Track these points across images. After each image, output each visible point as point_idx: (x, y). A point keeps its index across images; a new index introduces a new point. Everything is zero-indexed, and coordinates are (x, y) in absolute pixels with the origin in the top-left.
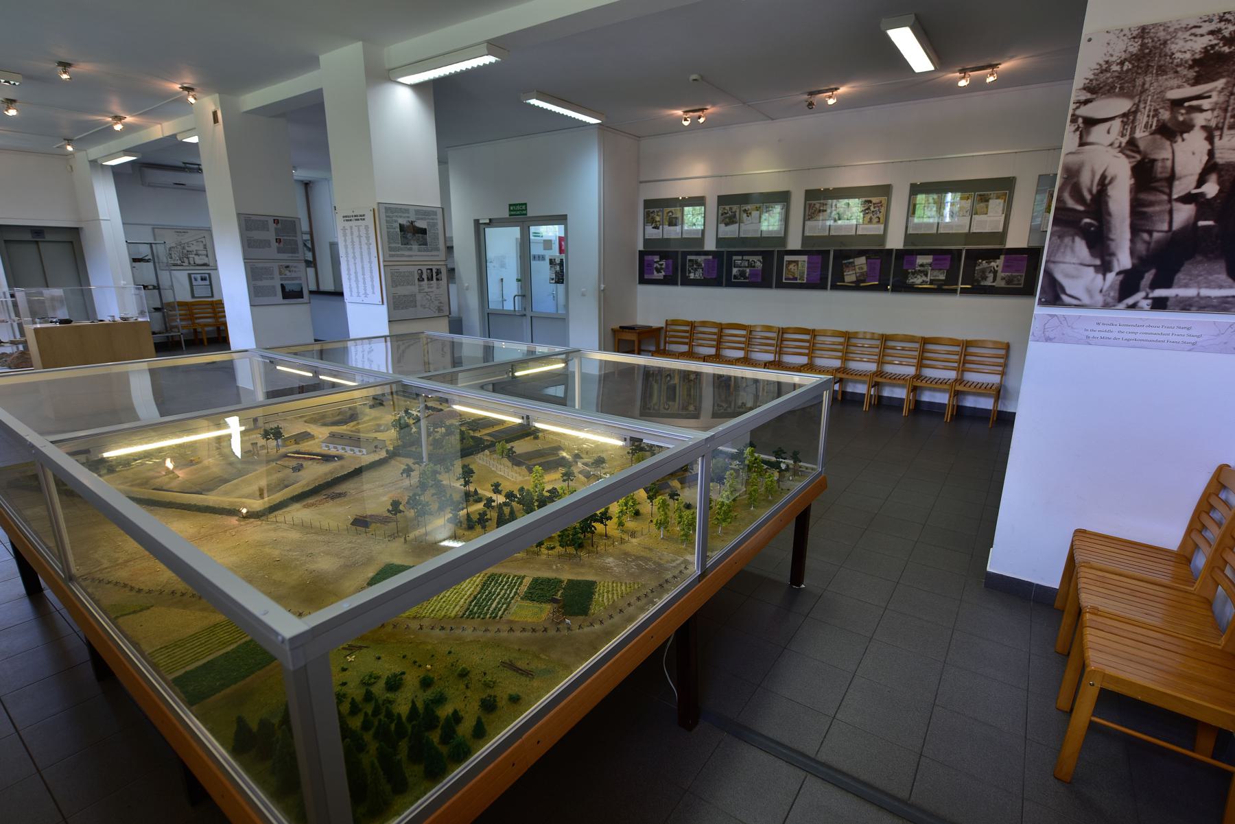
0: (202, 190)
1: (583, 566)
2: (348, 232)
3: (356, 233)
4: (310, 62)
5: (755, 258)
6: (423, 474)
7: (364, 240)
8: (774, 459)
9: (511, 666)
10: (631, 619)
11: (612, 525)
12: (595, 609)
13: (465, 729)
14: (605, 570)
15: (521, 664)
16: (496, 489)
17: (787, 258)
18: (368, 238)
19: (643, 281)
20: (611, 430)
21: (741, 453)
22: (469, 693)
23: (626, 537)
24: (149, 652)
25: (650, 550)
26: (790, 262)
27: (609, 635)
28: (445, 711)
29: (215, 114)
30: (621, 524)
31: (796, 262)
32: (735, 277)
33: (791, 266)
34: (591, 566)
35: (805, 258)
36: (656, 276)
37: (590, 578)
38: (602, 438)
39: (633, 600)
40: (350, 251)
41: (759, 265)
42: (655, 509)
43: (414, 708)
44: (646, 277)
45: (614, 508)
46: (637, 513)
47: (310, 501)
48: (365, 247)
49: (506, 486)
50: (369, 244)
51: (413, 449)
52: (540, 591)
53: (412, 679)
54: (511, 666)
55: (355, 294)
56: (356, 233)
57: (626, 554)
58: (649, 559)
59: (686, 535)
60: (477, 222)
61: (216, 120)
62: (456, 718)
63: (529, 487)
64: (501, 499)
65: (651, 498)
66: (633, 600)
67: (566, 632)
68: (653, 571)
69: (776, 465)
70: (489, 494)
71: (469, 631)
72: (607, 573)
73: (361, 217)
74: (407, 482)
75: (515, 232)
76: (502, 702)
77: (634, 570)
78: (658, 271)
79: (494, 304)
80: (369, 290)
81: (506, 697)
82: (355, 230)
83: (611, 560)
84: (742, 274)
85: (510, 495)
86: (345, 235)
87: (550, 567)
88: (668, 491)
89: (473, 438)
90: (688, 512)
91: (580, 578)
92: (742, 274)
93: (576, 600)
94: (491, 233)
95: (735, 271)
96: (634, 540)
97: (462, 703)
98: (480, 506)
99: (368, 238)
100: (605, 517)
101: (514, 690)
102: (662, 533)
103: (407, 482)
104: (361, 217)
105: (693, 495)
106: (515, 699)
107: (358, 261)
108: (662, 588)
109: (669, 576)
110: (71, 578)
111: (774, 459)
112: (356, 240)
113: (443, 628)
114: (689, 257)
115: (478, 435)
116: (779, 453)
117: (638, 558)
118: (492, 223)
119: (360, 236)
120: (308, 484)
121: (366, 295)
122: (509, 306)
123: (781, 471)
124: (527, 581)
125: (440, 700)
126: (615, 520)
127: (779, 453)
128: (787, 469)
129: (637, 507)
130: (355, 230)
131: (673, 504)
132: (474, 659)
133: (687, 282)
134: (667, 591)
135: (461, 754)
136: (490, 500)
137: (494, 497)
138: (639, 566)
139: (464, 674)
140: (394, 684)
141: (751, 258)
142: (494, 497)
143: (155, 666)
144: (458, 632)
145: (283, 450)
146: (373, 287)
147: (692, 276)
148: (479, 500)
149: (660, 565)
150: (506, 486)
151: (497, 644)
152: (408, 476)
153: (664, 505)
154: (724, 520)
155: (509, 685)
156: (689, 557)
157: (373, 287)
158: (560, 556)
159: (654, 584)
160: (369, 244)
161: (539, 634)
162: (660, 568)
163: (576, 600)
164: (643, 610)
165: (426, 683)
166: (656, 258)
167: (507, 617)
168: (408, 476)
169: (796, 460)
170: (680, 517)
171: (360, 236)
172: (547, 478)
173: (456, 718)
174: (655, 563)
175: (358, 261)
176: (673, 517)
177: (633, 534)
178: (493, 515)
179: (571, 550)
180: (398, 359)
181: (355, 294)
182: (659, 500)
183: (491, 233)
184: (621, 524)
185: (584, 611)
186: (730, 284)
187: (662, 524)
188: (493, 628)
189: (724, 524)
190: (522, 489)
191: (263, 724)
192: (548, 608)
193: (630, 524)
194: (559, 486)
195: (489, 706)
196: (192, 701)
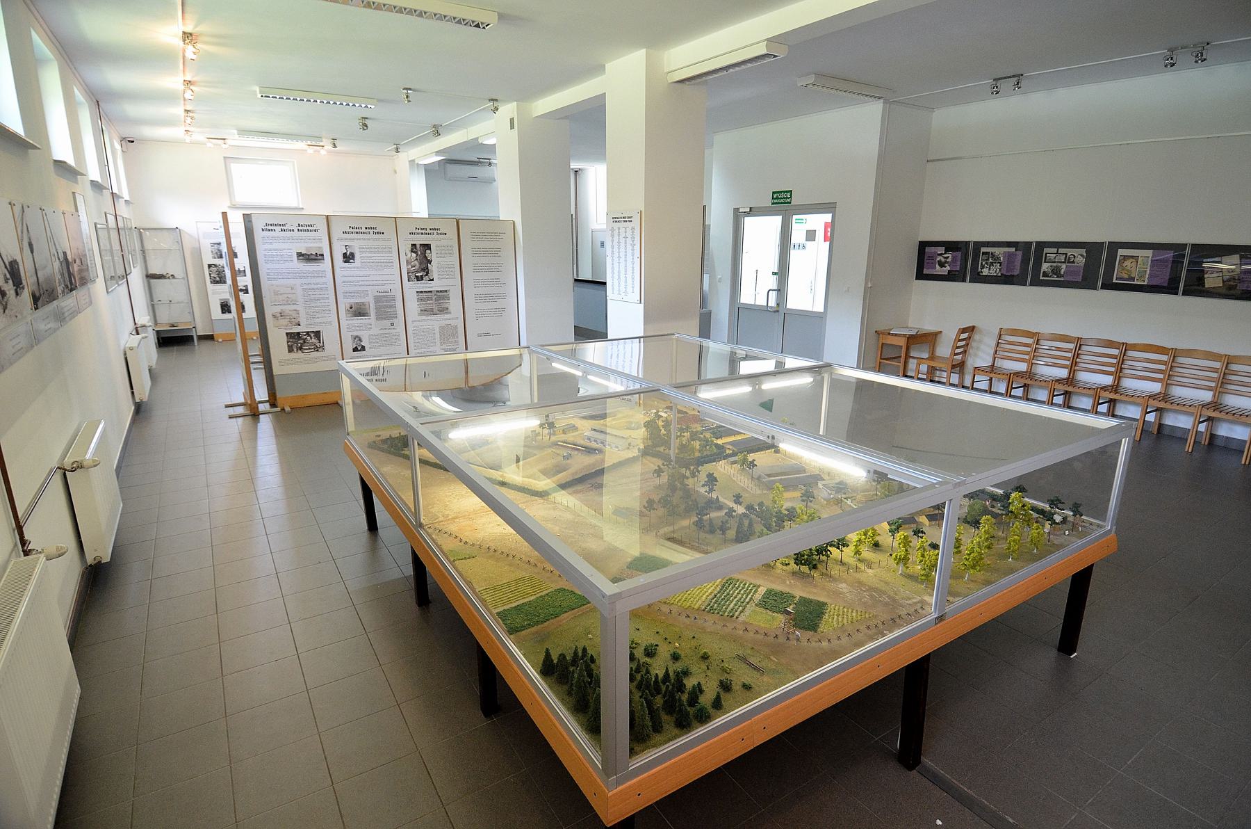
0: (490, 181)
1: (815, 586)
2: (616, 232)
3: (623, 235)
4: (600, 69)
5: (1076, 252)
6: (671, 477)
7: (629, 241)
8: (1047, 507)
9: (744, 660)
10: (859, 644)
11: (848, 552)
12: (822, 627)
13: (706, 699)
14: (837, 594)
15: (752, 660)
16: (738, 499)
17: (1121, 252)
18: (633, 239)
19: (920, 276)
20: (858, 462)
21: (1007, 496)
22: (709, 673)
23: (861, 566)
24: (482, 593)
25: (886, 583)
26: (1125, 258)
27: (836, 655)
28: (690, 683)
29: (512, 120)
30: (858, 552)
31: (1136, 258)
32: (1045, 274)
33: (1127, 263)
34: (824, 588)
35: (1149, 253)
36: (939, 270)
37: (822, 599)
38: (849, 467)
39: (863, 628)
40: (616, 249)
41: (1081, 261)
42: (896, 544)
43: (667, 675)
44: (925, 272)
45: (853, 537)
46: (876, 545)
47: (579, 487)
48: (629, 247)
49: (747, 498)
50: (633, 245)
51: (662, 449)
52: (773, 601)
53: (664, 652)
54: (744, 660)
55: (616, 291)
56: (623, 235)
57: (860, 583)
58: (884, 593)
59: (927, 575)
60: (736, 210)
61: (512, 127)
62: (698, 690)
63: (768, 503)
64: (741, 510)
65: (893, 532)
66: (863, 628)
67: (795, 642)
68: (886, 604)
69: (1048, 516)
70: (732, 504)
71: (710, 622)
72: (837, 594)
73: (628, 219)
74: (657, 481)
75: (777, 221)
76: (736, 686)
77: (867, 599)
78: (942, 265)
79: (746, 297)
80: (629, 290)
81: (740, 683)
82: (622, 230)
83: (844, 585)
84: (1056, 271)
85: (750, 508)
86: (613, 235)
87: (784, 582)
88: (914, 526)
89: (717, 445)
90: (932, 552)
91: (811, 597)
92: (1056, 271)
93: (808, 616)
94: (750, 223)
95: (1045, 267)
96: (869, 571)
97: (705, 680)
98: (722, 513)
99: (633, 239)
100: (841, 544)
101: (748, 681)
102: (901, 568)
103: (657, 481)
104: (628, 219)
105: (940, 535)
106: (747, 687)
107: (622, 260)
108: (894, 623)
109: (903, 612)
110: (421, 525)
111: (1047, 507)
112: (622, 241)
113: (688, 616)
114: (983, 249)
115: (720, 442)
116: (1054, 502)
117: (871, 589)
118: (752, 212)
119: (626, 237)
120: (576, 473)
121: (626, 293)
122: (761, 301)
123: (1054, 522)
124: (762, 590)
125: (686, 673)
126: (852, 548)
127: (1054, 502)
128: (1065, 520)
129: (877, 538)
130: (622, 230)
131: (916, 542)
132: (711, 646)
133: (978, 278)
134: (899, 626)
135: (703, 718)
136: (732, 510)
137: (735, 506)
138: (871, 596)
139: (705, 657)
140: (650, 652)
141: (1069, 252)
142: (735, 506)
143: (483, 601)
144: (700, 622)
145: (554, 438)
146: (633, 286)
147: (985, 272)
148: (720, 508)
149: (894, 600)
150: (747, 498)
151: (735, 639)
152: (659, 476)
153: (906, 541)
154: (973, 567)
155: (742, 674)
156: (927, 598)
157: (633, 286)
158: (794, 573)
159: (886, 617)
160: (633, 245)
161: (771, 639)
162: (893, 603)
163: (808, 616)
164: (872, 639)
165: (675, 657)
166: (941, 250)
167: (742, 618)
168: (659, 476)
169: (1076, 510)
170: (923, 556)
171: (626, 237)
172: (787, 495)
173: (698, 690)
174: (889, 597)
175: (622, 260)
176: (915, 556)
177: (869, 564)
178: (734, 524)
179: (805, 569)
180: (649, 360)
181: (616, 291)
182: (900, 535)
183: (750, 223)
184: (858, 552)
185: (813, 627)
186: (1036, 282)
187: (903, 560)
188: (730, 626)
189: (972, 571)
190: (761, 504)
191: (562, 657)
192: (781, 618)
193: (866, 553)
194: (799, 506)
195: (726, 687)
196: (512, 631)
